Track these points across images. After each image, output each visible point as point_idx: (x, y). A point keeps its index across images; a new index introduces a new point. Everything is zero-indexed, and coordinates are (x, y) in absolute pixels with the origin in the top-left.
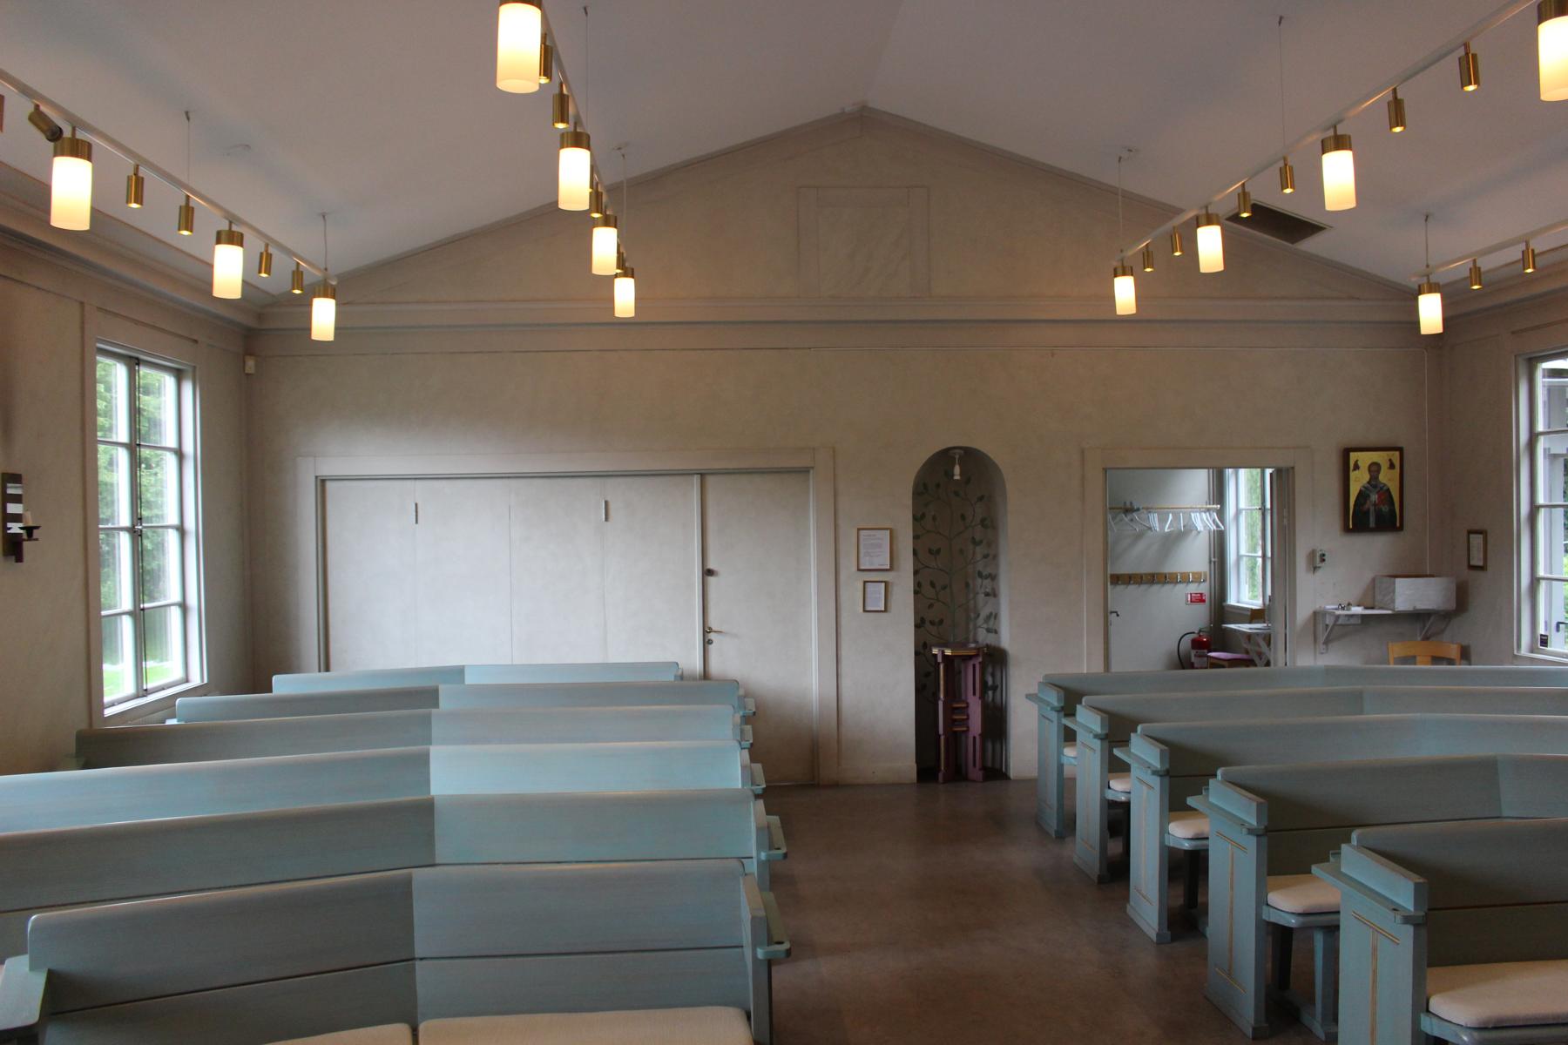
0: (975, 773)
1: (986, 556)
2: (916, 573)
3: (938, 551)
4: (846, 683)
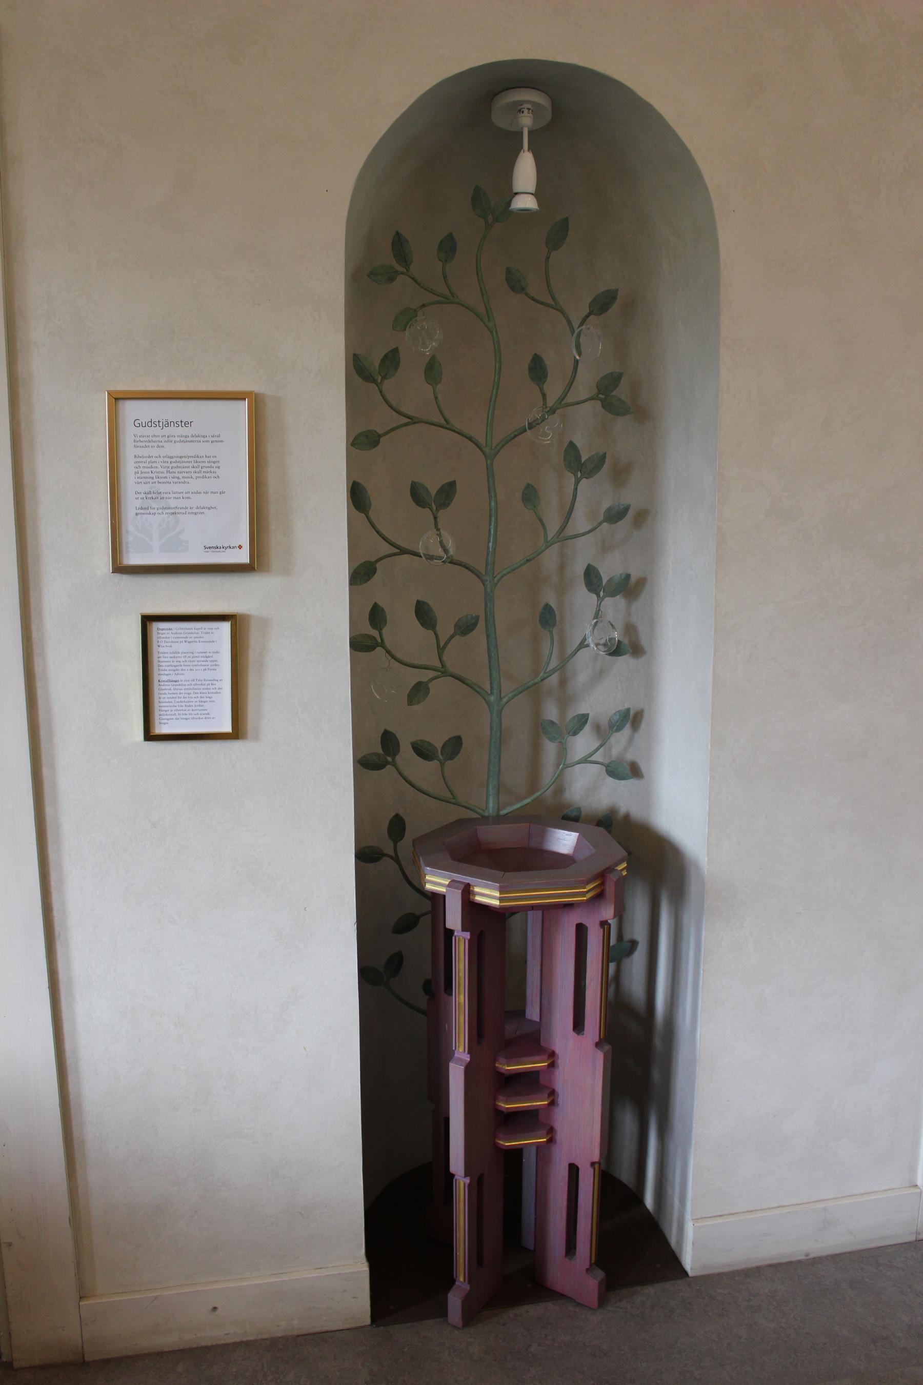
0: (573, 1269)
1: (615, 515)
2: (361, 574)
3: (448, 491)
4: (88, 1012)
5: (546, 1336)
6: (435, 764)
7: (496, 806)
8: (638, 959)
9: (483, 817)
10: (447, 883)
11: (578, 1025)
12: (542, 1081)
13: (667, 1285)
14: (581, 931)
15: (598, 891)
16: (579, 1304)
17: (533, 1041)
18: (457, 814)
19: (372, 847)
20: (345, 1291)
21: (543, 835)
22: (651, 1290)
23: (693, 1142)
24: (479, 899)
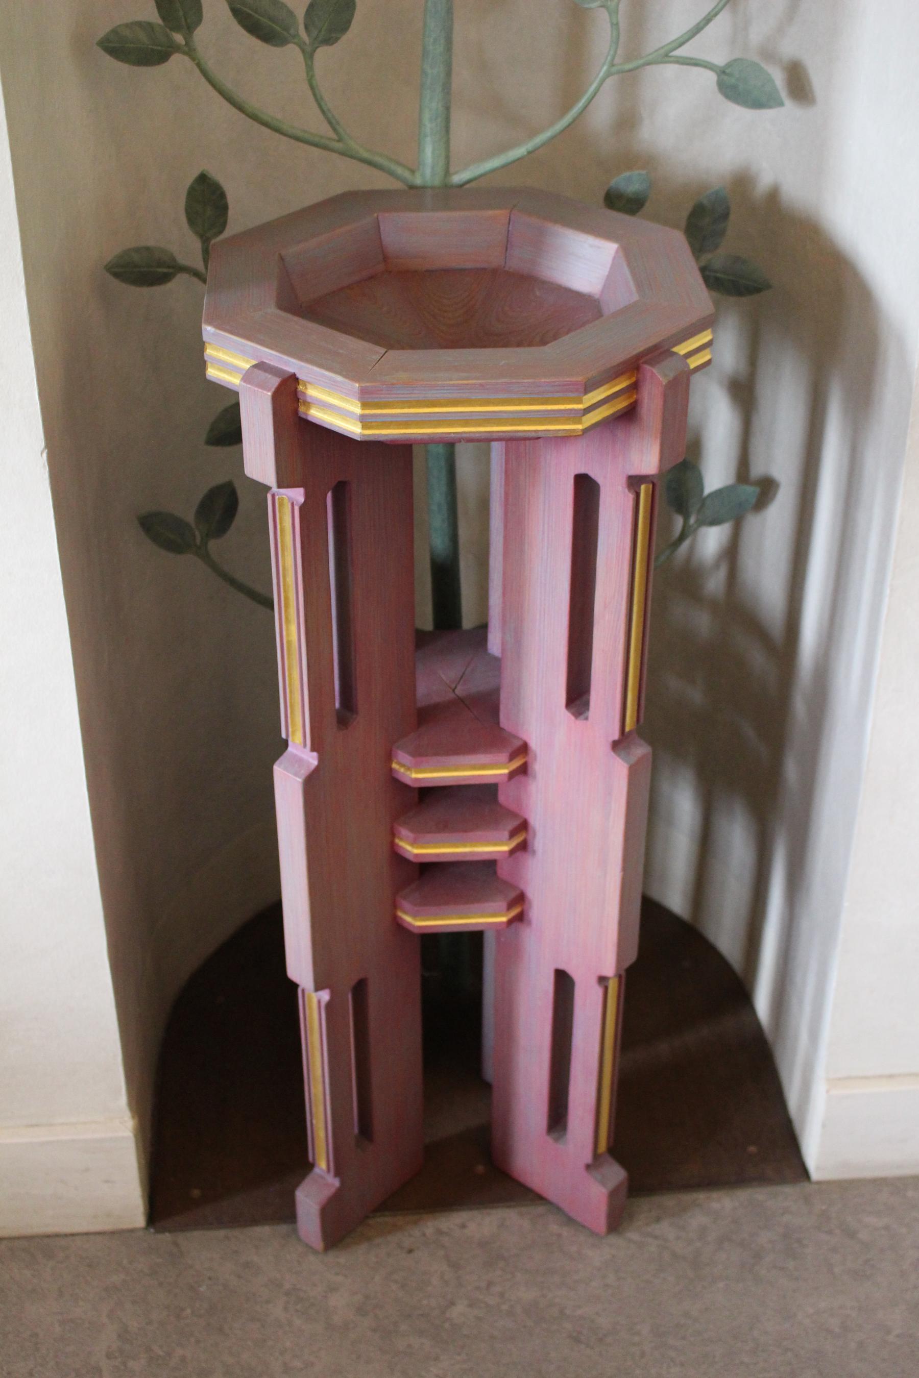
0: (564, 1158)
5: (490, 1284)
6: (292, 52)
7: (442, 163)
8: (776, 521)
9: (412, 187)
10: (247, 366)
11: (577, 694)
12: (502, 798)
13: (760, 1194)
14: (586, 491)
15: (621, 404)
16: (570, 1221)
17: (481, 717)
18: (349, 177)
19: (147, 249)
20: (87, 1170)
21: (539, 243)
22: (724, 1204)
23: (841, 936)
24: (317, 415)
